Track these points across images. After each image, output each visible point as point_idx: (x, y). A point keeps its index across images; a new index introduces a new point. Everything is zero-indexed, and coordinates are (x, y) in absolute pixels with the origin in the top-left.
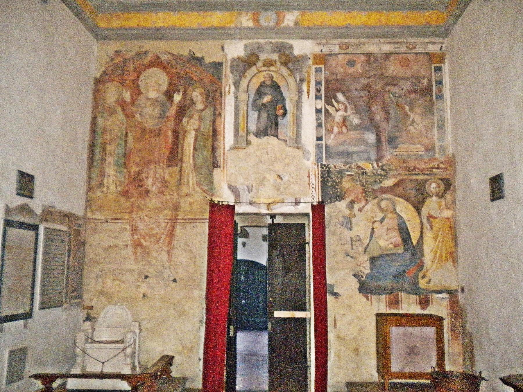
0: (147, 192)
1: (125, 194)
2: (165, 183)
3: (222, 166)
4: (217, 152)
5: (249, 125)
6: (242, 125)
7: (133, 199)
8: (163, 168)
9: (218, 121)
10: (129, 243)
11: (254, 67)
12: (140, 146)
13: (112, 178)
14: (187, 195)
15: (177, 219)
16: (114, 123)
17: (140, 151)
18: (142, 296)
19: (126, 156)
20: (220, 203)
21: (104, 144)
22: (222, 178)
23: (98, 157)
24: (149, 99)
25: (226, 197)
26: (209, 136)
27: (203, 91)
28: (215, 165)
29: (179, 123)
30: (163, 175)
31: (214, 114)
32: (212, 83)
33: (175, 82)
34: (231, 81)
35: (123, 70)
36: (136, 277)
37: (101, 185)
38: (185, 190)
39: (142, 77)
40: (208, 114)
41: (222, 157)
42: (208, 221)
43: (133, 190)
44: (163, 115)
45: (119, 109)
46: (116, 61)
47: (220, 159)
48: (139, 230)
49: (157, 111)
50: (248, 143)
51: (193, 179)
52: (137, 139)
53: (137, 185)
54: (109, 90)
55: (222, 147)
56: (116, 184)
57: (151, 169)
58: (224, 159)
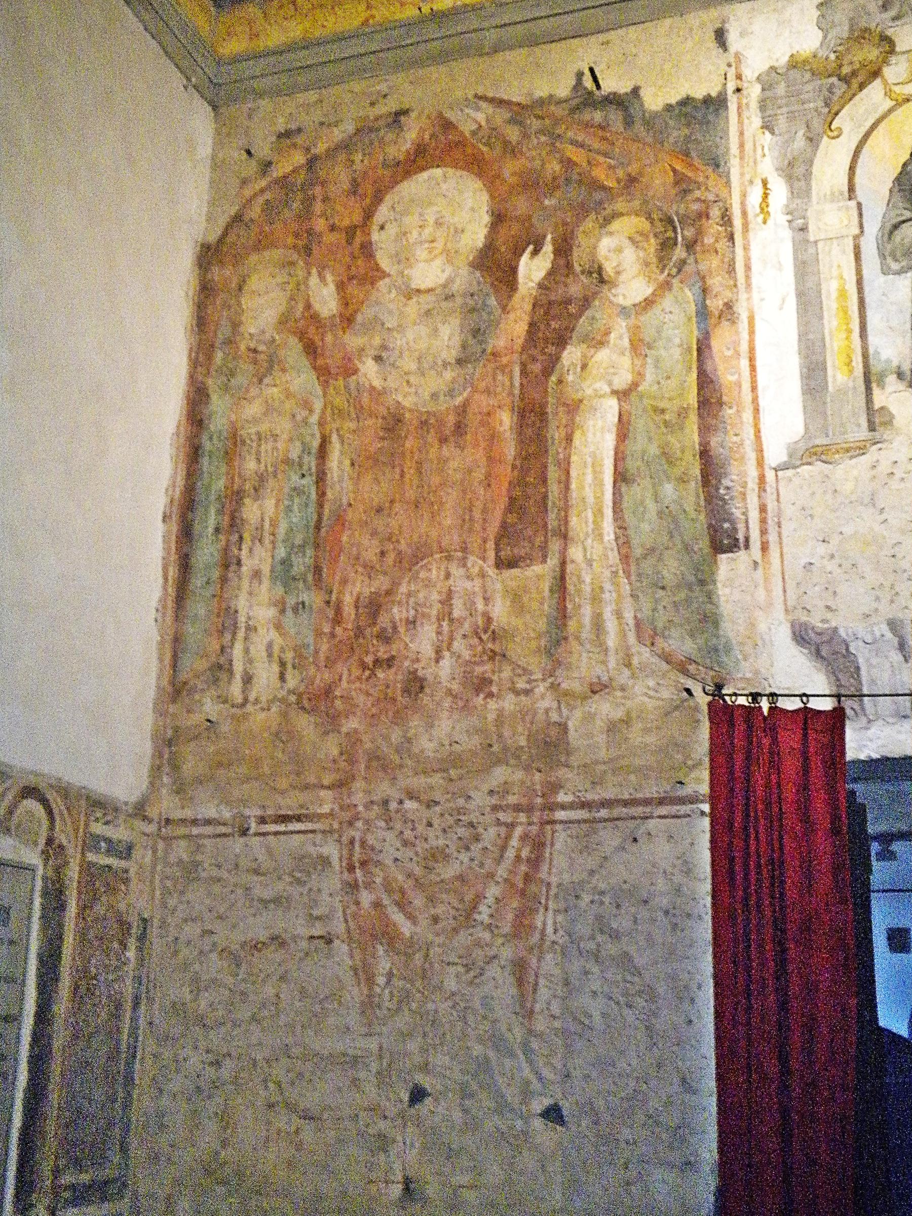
0: (416, 685)
1: (319, 701)
2: (491, 640)
3: (755, 535)
4: (726, 482)
5: (872, 339)
6: (838, 341)
7: (352, 724)
8: (483, 575)
9: (719, 344)
10: (338, 927)
11: (875, 90)
12: (375, 490)
13: (266, 635)
14: (597, 688)
15: (552, 807)
16: (275, 411)
17: (379, 510)
18: (397, 1190)
19: (323, 534)
20: (765, 705)
21: (235, 498)
22: (761, 594)
23: (207, 552)
24: (411, 293)
25: (794, 678)
26: (682, 413)
27: (642, 223)
28: (724, 540)
29: (547, 372)
30: (480, 606)
31: (703, 313)
32: (683, 185)
33: (521, 205)
34: (767, 167)
35: (308, 201)
36: (371, 1090)
37: (220, 669)
38: (584, 665)
39: (383, 212)
40: (675, 320)
41: (753, 502)
42: (706, 808)
43: (347, 679)
44: (474, 350)
45: (293, 351)
46: (282, 169)
47: (746, 511)
48: (378, 863)
49: (448, 336)
50: (877, 420)
51: (619, 615)
52: (364, 463)
53: (369, 659)
54: (254, 283)
55: (752, 456)
56: (282, 664)
57: (428, 584)
58: (763, 509)
